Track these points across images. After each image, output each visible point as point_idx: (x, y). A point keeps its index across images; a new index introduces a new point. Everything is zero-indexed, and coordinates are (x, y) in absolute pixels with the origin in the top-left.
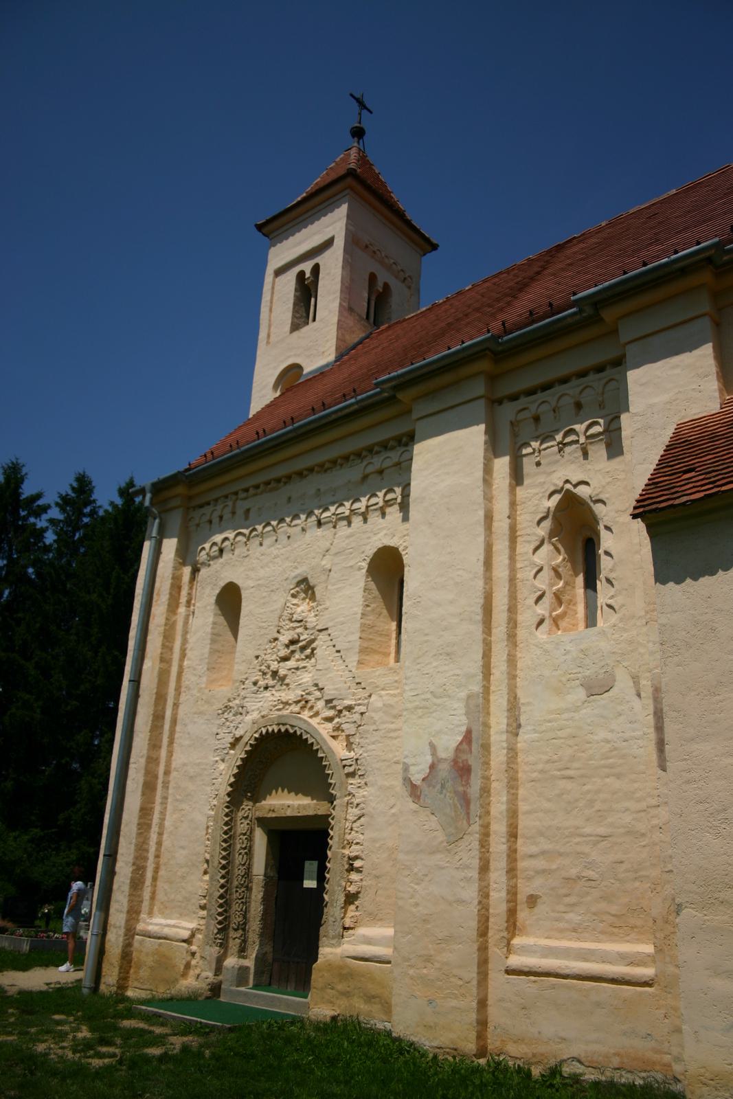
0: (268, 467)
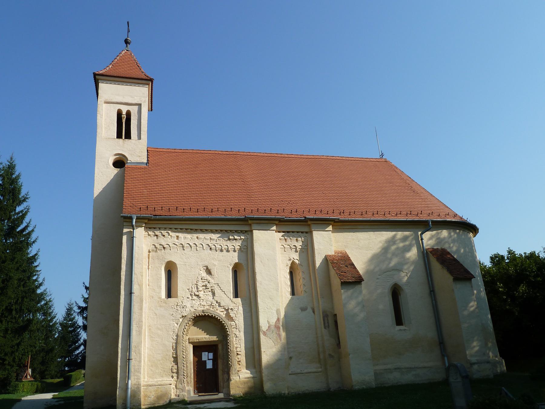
0: (173, 223)
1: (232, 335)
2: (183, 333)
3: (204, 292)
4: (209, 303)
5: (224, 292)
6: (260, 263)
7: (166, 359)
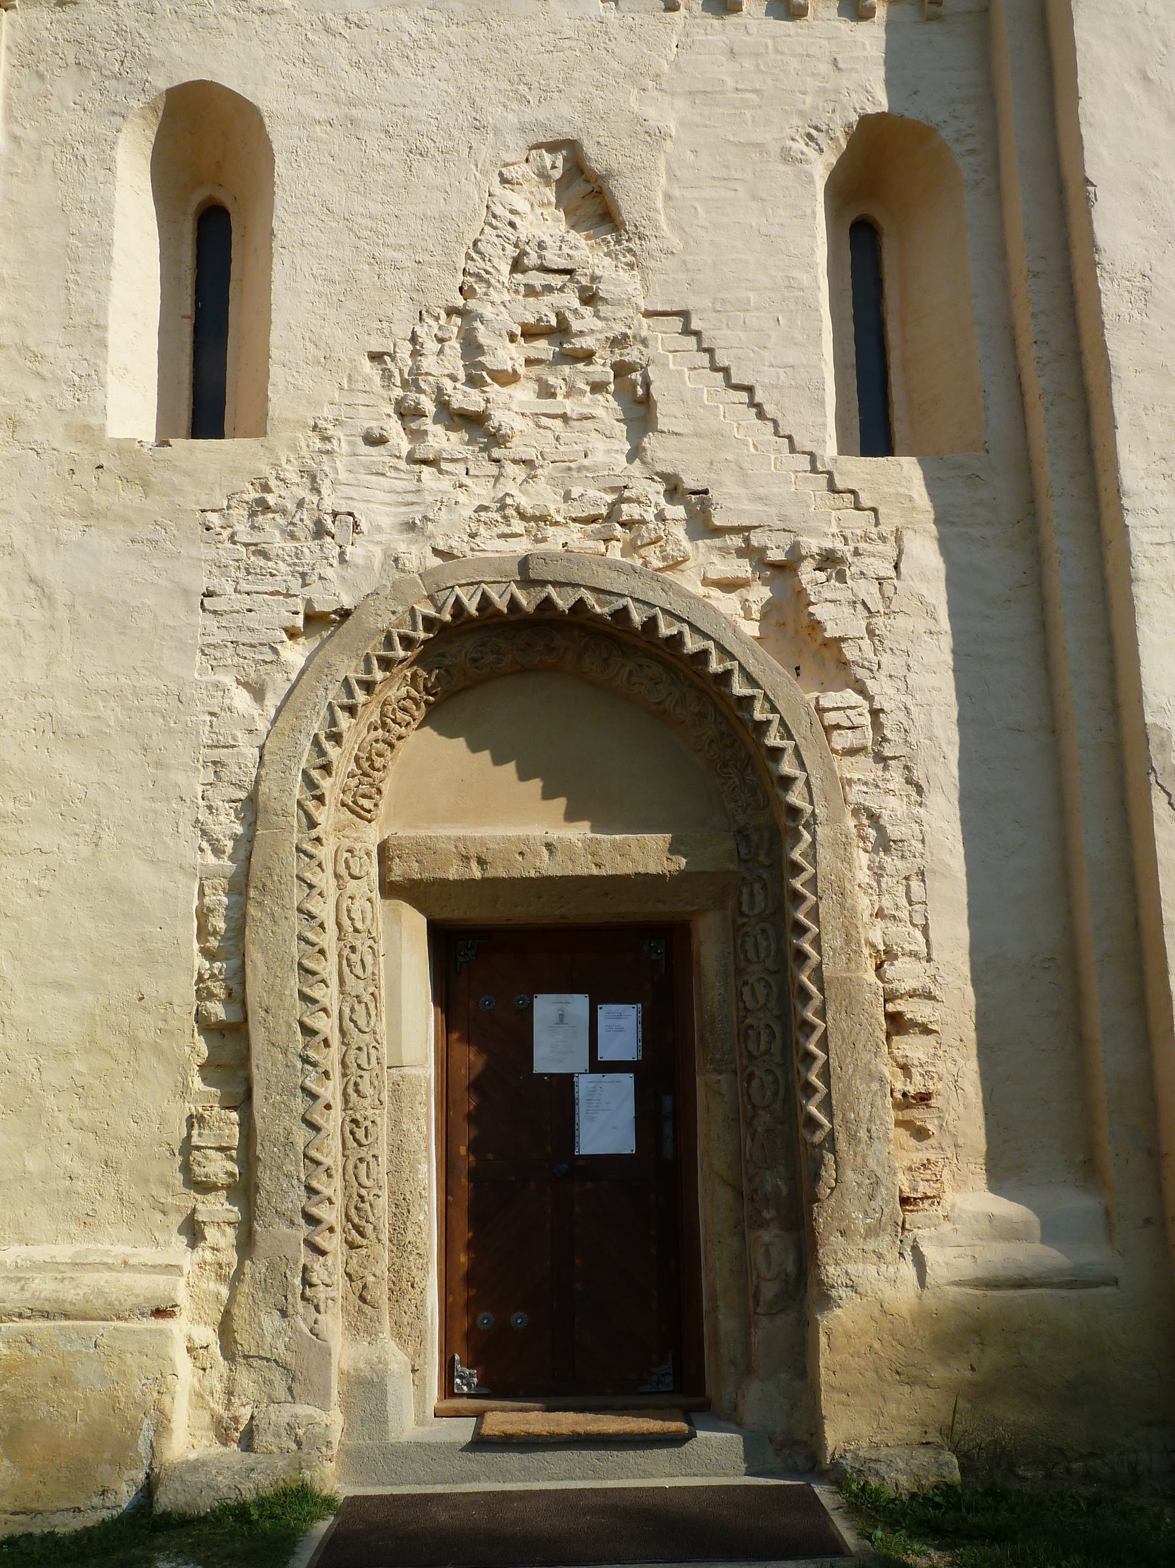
1: (835, 820)
2: (310, 783)
3: (547, 392)
4: (592, 493)
5: (744, 396)
6: (1129, 88)
7: (135, 1044)
